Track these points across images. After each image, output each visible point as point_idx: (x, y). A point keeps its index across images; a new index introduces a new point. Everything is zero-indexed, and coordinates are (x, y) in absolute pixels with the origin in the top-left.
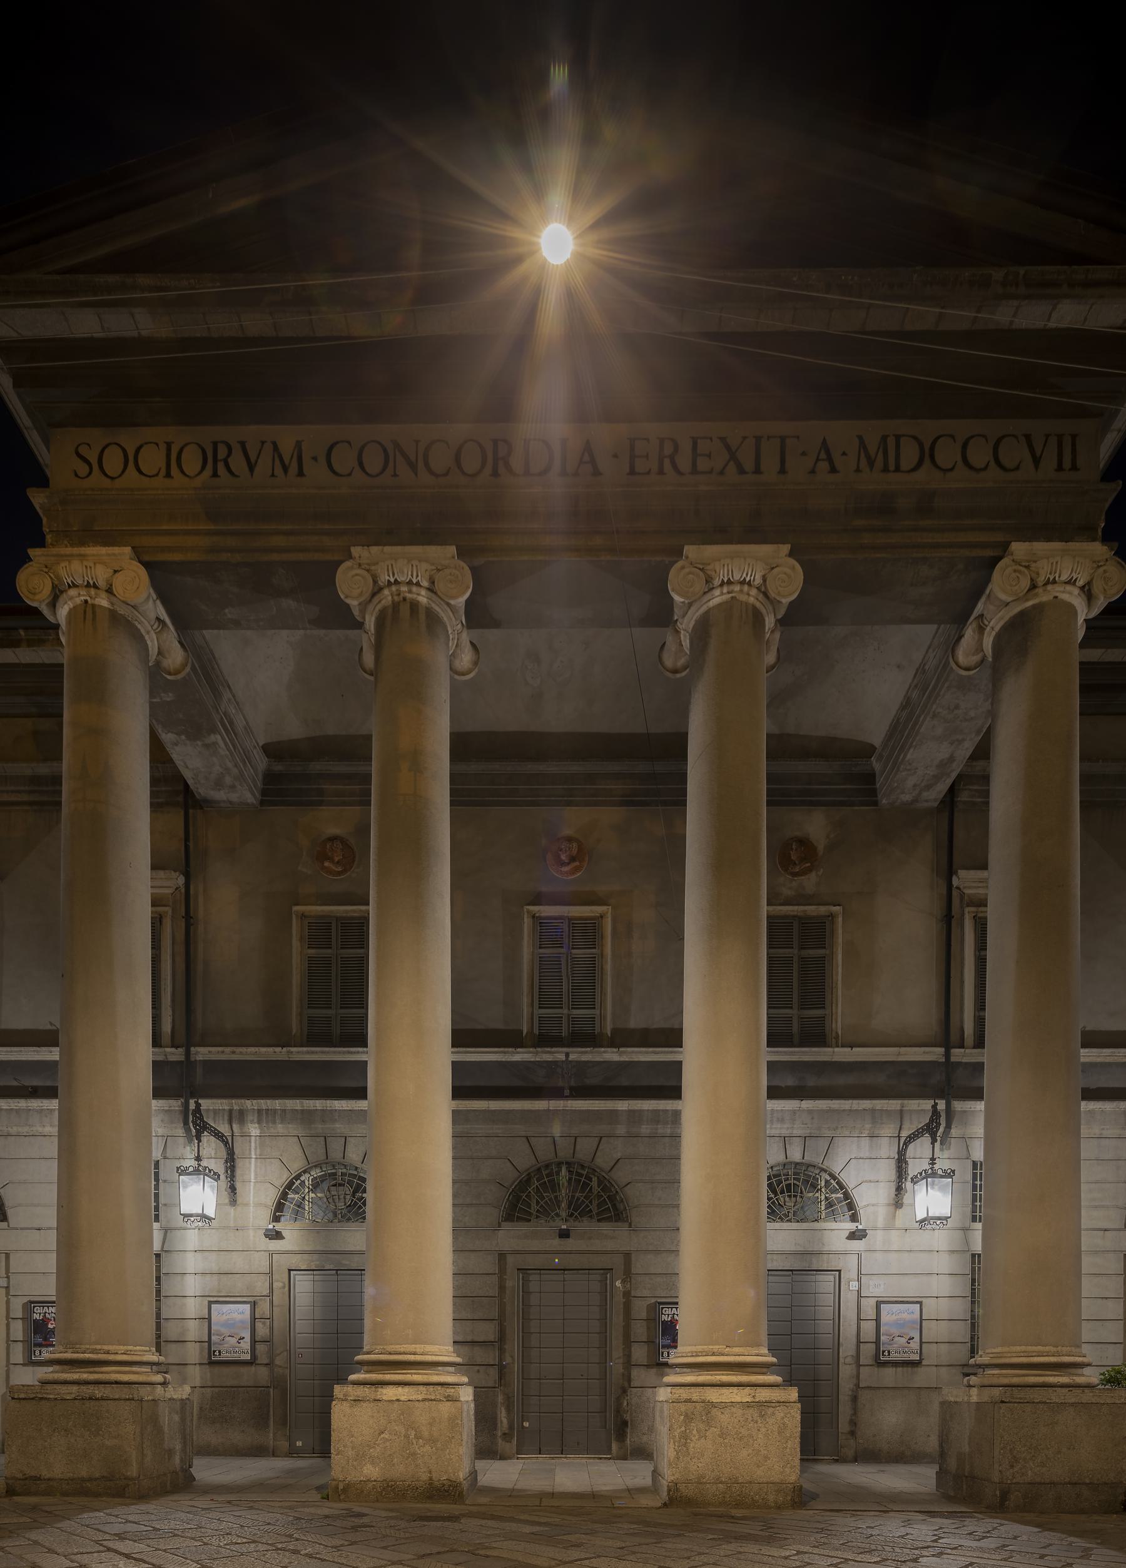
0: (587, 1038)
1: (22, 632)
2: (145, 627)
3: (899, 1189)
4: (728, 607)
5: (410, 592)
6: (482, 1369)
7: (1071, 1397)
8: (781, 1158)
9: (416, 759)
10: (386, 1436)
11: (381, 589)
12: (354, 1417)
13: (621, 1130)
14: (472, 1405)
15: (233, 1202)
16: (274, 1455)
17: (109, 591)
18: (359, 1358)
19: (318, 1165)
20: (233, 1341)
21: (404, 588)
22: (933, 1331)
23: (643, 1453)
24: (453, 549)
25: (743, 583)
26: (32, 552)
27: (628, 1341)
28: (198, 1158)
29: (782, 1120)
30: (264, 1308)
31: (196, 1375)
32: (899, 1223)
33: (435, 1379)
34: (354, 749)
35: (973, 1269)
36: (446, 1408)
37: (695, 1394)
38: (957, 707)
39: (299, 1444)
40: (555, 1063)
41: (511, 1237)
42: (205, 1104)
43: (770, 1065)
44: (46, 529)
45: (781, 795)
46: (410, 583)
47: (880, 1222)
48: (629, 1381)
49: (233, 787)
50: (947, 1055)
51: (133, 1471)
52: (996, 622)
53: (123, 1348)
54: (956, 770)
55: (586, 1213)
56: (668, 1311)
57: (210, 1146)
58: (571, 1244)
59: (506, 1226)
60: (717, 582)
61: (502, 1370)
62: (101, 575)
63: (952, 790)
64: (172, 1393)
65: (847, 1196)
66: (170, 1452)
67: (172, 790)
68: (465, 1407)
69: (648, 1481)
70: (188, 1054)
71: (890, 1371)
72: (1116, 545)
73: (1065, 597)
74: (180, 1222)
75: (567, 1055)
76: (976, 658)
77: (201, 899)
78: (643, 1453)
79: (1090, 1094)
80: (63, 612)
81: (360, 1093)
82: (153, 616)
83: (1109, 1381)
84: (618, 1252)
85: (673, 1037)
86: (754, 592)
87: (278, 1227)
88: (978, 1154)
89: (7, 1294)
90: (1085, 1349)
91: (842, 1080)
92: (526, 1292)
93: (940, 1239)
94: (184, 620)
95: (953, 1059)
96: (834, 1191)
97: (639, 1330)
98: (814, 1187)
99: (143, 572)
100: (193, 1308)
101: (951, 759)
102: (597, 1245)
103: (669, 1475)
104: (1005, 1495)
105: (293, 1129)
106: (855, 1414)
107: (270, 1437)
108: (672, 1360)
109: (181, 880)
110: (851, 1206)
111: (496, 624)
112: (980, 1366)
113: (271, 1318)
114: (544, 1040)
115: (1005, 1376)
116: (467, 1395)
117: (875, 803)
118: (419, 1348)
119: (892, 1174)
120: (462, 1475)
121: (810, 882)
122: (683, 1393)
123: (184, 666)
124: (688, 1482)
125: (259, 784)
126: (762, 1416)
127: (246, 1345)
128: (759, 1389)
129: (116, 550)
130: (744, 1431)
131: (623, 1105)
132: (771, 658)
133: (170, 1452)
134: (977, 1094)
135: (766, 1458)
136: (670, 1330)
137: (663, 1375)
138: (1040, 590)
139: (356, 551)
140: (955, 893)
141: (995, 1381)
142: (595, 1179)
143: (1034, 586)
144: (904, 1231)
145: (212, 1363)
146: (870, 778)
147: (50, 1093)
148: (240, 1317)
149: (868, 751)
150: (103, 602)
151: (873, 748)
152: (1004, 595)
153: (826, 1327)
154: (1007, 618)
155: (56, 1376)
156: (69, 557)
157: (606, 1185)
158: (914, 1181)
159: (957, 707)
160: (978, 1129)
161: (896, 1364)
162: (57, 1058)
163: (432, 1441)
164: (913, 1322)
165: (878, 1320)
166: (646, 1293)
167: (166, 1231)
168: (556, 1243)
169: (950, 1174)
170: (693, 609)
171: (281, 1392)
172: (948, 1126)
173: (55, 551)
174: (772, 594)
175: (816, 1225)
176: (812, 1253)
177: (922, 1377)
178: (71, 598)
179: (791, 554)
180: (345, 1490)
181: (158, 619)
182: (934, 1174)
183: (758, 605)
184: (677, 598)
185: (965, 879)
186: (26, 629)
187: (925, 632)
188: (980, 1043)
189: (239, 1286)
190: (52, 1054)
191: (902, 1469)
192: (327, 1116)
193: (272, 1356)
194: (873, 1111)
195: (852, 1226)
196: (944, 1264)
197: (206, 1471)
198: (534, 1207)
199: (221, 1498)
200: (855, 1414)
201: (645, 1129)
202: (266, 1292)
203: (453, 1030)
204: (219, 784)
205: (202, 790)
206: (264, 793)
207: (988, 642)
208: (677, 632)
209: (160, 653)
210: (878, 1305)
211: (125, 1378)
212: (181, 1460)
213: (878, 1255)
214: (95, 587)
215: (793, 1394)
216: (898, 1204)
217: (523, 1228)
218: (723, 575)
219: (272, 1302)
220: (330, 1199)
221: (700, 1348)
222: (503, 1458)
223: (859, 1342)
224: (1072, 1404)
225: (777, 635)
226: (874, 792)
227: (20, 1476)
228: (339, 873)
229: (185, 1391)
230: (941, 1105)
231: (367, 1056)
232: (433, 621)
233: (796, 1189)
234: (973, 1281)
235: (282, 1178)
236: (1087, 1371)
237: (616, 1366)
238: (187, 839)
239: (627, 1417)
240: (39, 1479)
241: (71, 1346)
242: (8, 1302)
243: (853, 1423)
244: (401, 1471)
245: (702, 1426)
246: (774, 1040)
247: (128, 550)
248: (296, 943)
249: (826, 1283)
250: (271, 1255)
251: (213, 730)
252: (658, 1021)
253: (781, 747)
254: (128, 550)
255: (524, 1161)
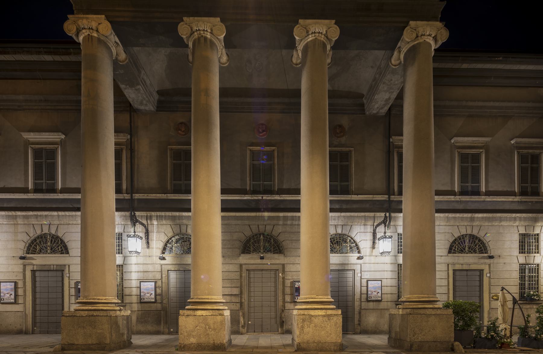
0: (270, 192)
1: (72, 50)
2: (111, 45)
3: (374, 243)
4: (314, 41)
5: (204, 33)
6: (235, 304)
7: (433, 312)
8: (335, 232)
9: (207, 92)
10: (198, 328)
11: (194, 32)
12: (187, 322)
13: (281, 223)
14: (229, 317)
15: (148, 247)
16: (163, 334)
17: (97, 31)
18: (189, 300)
19: (177, 235)
20: (149, 295)
21: (202, 32)
22: (386, 290)
23: (289, 332)
24: (219, 19)
25: (319, 33)
26: (69, 16)
27: (284, 294)
28: (135, 232)
29: (335, 220)
30: (159, 283)
31: (135, 307)
32: (374, 254)
33: (215, 308)
34: (187, 93)
35: (398, 269)
36: (219, 318)
37: (306, 312)
38: (391, 80)
39: (172, 330)
40: (258, 200)
41: (244, 259)
42: (137, 213)
43: (331, 201)
44: (74, 9)
45: (332, 111)
46: (204, 30)
47: (368, 254)
48: (285, 307)
49: (146, 105)
50: (389, 198)
51: (108, 341)
52: (404, 50)
53: (104, 298)
54: (391, 102)
55: (269, 251)
56: (297, 284)
57: (139, 229)
58: (264, 261)
59: (242, 255)
60: (310, 32)
61: (241, 303)
62: (94, 25)
63: (389, 109)
64: (123, 313)
65: (357, 245)
66: (123, 334)
67: (122, 105)
68: (226, 317)
69: (290, 342)
70: (132, 196)
71: (371, 303)
72: (444, 23)
73: (428, 40)
74: (128, 254)
75: (262, 197)
76: (398, 62)
77: (136, 143)
78: (289, 332)
79: (438, 211)
80: (81, 38)
81: (189, 210)
82: (113, 40)
83: (445, 306)
84: (280, 264)
85: (297, 191)
86: (323, 36)
87: (164, 256)
88: (400, 230)
89: (69, 279)
90: (437, 296)
91: (355, 206)
92: (249, 278)
93: (388, 259)
94: (126, 43)
95: (391, 199)
96: (352, 243)
97: (288, 290)
98: (346, 242)
99: (109, 24)
100: (134, 284)
101: (389, 98)
102: (274, 261)
103: (297, 340)
104: (411, 346)
105: (169, 222)
106: (360, 318)
107: (162, 328)
108: (298, 301)
109: (129, 137)
110: (358, 248)
111: (235, 47)
112: (402, 302)
113: (162, 287)
114: (254, 192)
115: (411, 305)
116: (227, 313)
117: (364, 114)
118: (209, 297)
119: (372, 238)
120: (225, 341)
121: (343, 140)
122: (302, 312)
123: (126, 59)
124: (304, 343)
125: (156, 104)
126: (329, 320)
127: (153, 296)
128: (328, 310)
129: (99, 16)
130: (323, 325)
131: (281, 214)
132: (329, 61)
133: (123, 334)
134: (400, 211)
135: (331, 334)
136: (298, 290)
137: (296, 305)
138: (419, 38)
139: (185, 19)
140: (391, 144)
141: (408, 307)
142: (272, 239)
143: (417, 37)
144: (375, 258)
145: (141, 303)
146: (363, 105)
147: (78, 209)
148: (151, 287)
149: (362, 96)
150: (95, 35)
151: (364, 95)
152: (407, 36)
153: (350, 289)
154: (408, 48)
155: (80, 308)
156: (83, 18)
157: (276, 241)
158: (379, 239)
159: (391, 80)
160: (400, 222)
161: (373, 301)
162: (80, 197)
163: (214, 329)
164: (379, 287)
165: (367, 286)
166: (290, 278)
167: (125, 257)
168: (259, 261)
169: (391, 237)
170: (302, 42)
171: (163, 312)
172: (390, 222)
173: (77, 16)
174: (329, 37)
175: (346, 255)
176: (345, 264)
177: (382, 305)
178: (84, 33)
179: (335, 23)
180: (184, 347)
181: (115, 42)
182: (386, 237)
183: (324, 41)
184: (297, 38)
185: (395, 139)
186: (73, 49)
187: (380, 54)
188: (400, 193)
189: (150, 276)
190: (79, 196)
191: (376, 336)
192: (180, 218)
193: (162, 299)
194: (365, 216)
195: (359, 255)
196: (389, 267)
197: (137, 340)
198: (252, 249)
199: (139, 350)
200: (360, 318)
201: (289, 222)
202: (160, 278)
203: (221, 189)
204: (141, 103)
205: (136, 106)
206: (157, 107)
207: (402, 56)
208: (297, 51)
209: (117, 54)
210: (367, 281)
211: (105, 308)
212: (127, 337)
213: (367, 265)
214: (92, 29)
215: (340, 312)
216: (373, 247)
217: (248, 256)
218: (312, 30)
219: (162, 282)
220: (182, 246)
221: (307, 296)
222: (242, 334)
223: (361, 294)
224: (434, 315)
225: (331, 53)
226: (364, 110)
227: (66, 343)
228: (184, 135)
229: (128, 313)
230: (388, 214)
231: (191, 197)
232: (212, 45)
233: (340, 243)
234: (398, 273)
235: (165, 239)
236: (438, 303)
237: (281, 303)
238: (131, 122)
239: (284, 320)
240: (74, 344)
241: (86, 297)
242: (69, 282)
243: (359, 321)
244: (203, 340)
245: (308, 323)
246: (332, 192)
247: (103, 16)
248: (169, 159)
249: (350, 274)
250: (161, 265)
251: (138, 84)
252: (293, 186)
253: (332, 95)
254: (103, 16)
255: (248, 233)
